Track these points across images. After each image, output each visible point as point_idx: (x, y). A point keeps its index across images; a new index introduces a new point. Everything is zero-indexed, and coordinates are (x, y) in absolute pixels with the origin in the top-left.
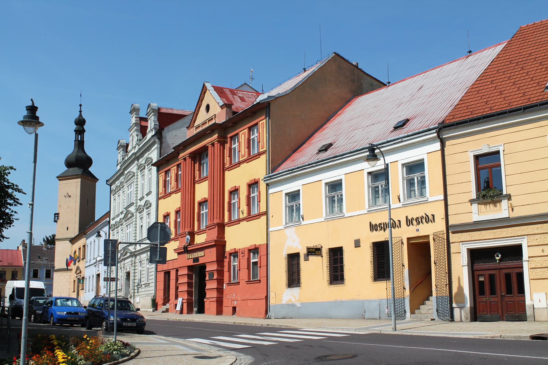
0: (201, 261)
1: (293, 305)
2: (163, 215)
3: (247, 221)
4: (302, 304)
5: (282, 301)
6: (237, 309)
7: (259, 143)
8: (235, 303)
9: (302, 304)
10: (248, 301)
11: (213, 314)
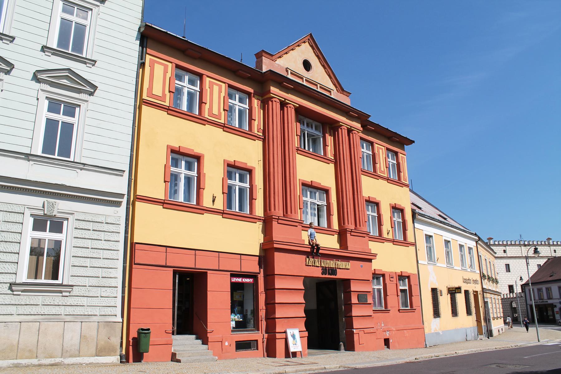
0: (341, 275)
1: (438, 334)
2: (203, 155)
3: (147, 88)
4: (443, 332)
5: (432, 330)
6: (391, 341)
7: (547, 342)
8: (387, 334)
9: (443, 332)
10: (405, 330)
11: (383, 349)
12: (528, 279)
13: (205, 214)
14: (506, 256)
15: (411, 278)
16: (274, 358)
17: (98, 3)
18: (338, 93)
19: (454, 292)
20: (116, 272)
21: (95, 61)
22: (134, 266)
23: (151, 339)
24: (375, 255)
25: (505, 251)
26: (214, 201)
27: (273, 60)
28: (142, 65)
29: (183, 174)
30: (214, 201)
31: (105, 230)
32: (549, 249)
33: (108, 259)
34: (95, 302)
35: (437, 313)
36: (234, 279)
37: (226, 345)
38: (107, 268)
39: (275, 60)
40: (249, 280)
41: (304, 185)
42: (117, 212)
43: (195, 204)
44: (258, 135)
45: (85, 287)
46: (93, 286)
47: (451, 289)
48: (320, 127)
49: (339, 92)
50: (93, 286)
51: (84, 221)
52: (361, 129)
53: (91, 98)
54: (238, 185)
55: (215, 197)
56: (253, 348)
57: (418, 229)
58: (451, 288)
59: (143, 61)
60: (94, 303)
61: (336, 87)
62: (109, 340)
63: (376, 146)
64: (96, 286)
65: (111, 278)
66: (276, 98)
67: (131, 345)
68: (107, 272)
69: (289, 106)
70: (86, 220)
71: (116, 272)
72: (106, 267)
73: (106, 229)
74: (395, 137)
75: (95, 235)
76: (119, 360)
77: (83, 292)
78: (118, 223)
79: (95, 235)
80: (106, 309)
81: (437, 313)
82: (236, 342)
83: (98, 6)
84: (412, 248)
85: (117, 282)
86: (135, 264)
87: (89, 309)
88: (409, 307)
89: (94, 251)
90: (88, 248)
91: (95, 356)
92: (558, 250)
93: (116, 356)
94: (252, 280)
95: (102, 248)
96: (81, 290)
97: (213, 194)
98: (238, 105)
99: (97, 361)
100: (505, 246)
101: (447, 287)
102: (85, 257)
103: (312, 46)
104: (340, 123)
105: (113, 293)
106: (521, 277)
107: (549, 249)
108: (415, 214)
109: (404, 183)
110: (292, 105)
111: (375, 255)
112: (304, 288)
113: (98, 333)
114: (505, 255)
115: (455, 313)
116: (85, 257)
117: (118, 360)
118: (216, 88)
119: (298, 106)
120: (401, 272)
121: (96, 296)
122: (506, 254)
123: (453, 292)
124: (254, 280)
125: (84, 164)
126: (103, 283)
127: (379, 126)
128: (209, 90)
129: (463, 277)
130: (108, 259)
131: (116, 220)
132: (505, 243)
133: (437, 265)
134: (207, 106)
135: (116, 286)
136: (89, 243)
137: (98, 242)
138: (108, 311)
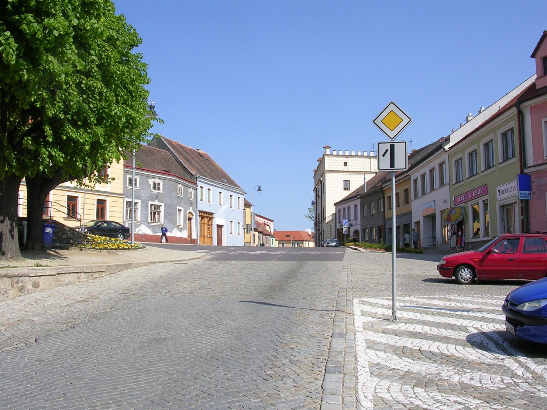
12: (364, 183)
14: (346, 170)
16: (339, 262)
25: (346, 164)
32: (369, 162)
66: (169, 150)
92: (341, 166)
100: (347, 157)
106: (259, 187)
107: (369, 162)
108: (76, 214)
114: (345, 169)
122: (347, 167)
132: (347, 153)
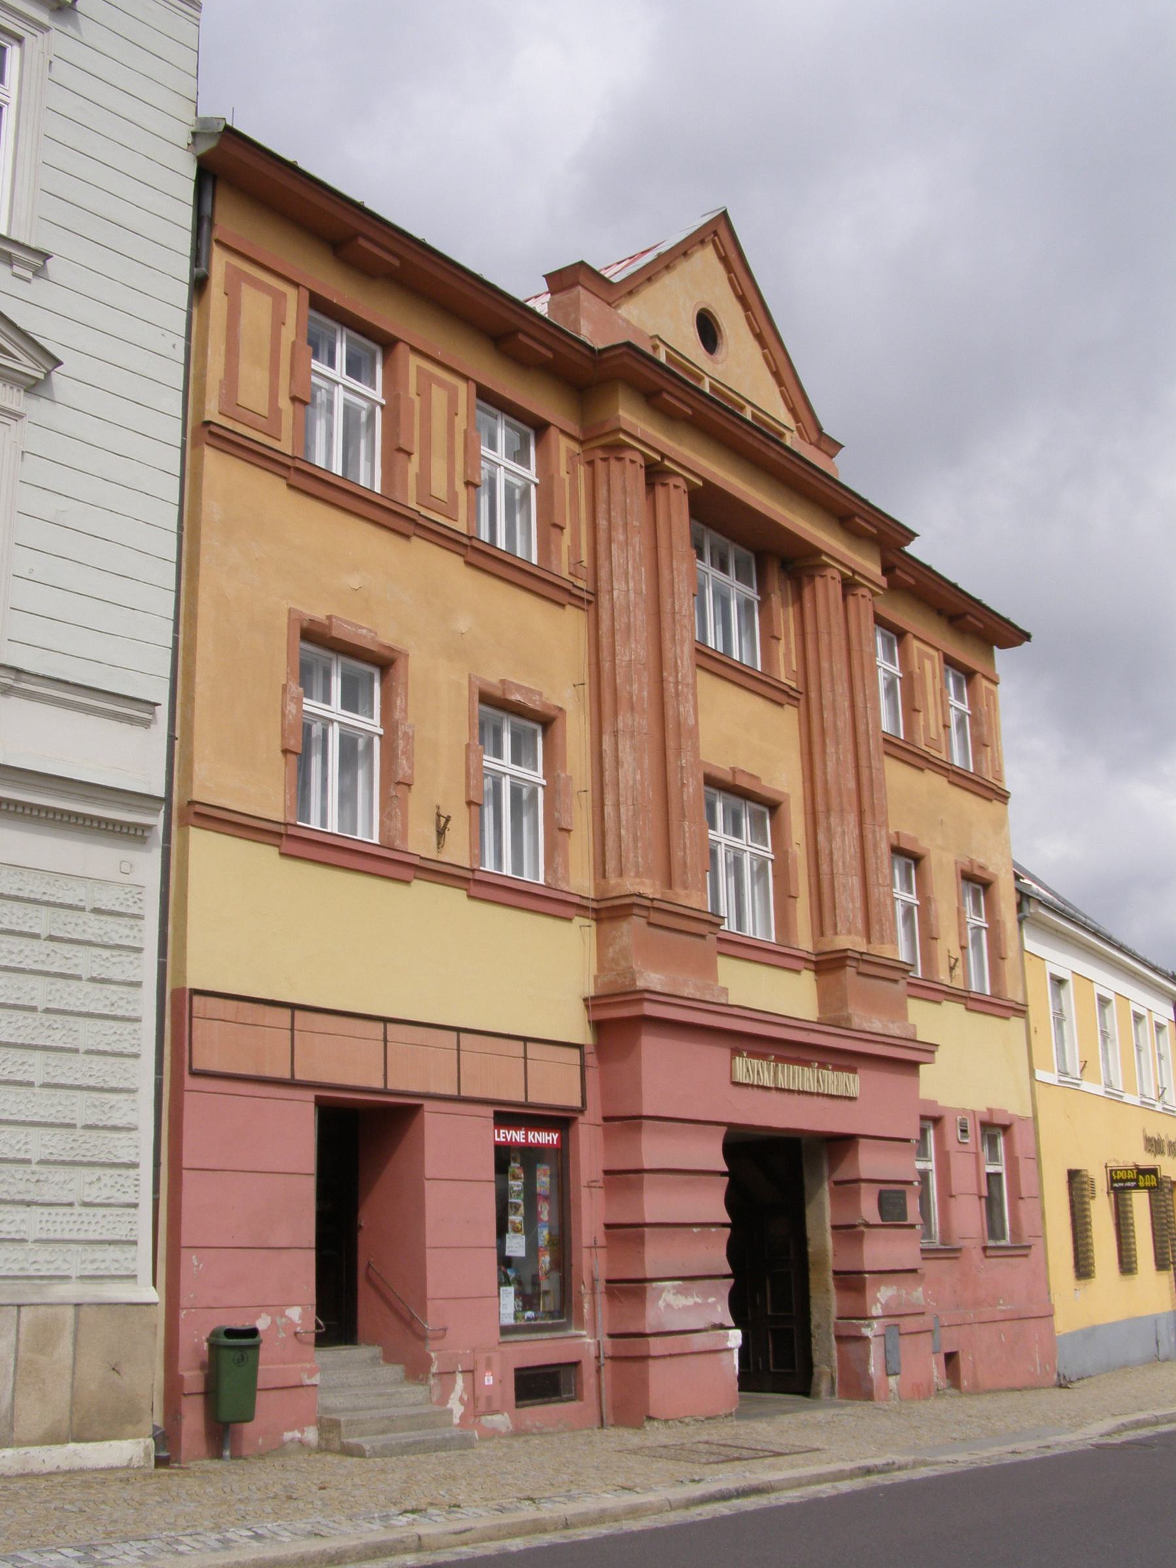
13: (415, 882)
15: (1016, 1129)
17: (43, 17)
18: (802, 441)
19: (1133, 1184)
20: (133, 1106)
21: (46, 254)
22: (189, 1082)
23: (260, 1367)
24: (930, 1049)
26: (441, 833)
27: (611, 301)
28: (199, 285)
29: (336, 724)
30: (441, 833)
31: (93, 939)
33: (104, 1053)
34: (61, 1224)
35: (1083, 1268)
36: (502, 1131)
37: (486, 1383)
38: (102, 1090)
39: (616, 303)
40: (547, 1138)
41: (712, 781)
42: (131, 866)
43: (378, 843)
44: (575, 586)
45: (22, 1167)
46: (55, 1163)
47: (1120, 1175)
48: (749, 564)
49: (804, 440)
50: (55, 1163)
51: (17, 899)
52: (883, 582)
53: (34, 408)
54: (511, 776)
55: (448, 819)
56: (564, 1394)
57: (1032, 957)
58: (1121, 1170)
59: (203, 269)
60: (58, 1227)
61: (797, 419)
62: (116, 1375)
63: (915, 645)
64: (64, 1163)
65: (115, 1128)
67: (584, 1250)
68: (103, 1104)
69: (672, 481)
70: (25, 894)
71: (133, 1106)
72: (99, 1085)
73: (93, 934)
74: (972, 615)
75: (59, 959)
76: (150, 1455)
77: (22, 1186)
78: (134, 910)
79: (59, 959)
80: (99, 1253)
81: (1083, 1268)
82: (517, 1370)
83: (45, 28)
84: (1016, 1023)
85: (137, 1147)
86: (195, 1074)
87: (44, 1254)
88: (1008, 1238)
89: (55, 1021)
90: (33, 1009)
91: (68, 1442)
93: (141, 1440)
94: (556, 1136)
95: (83, 1009)
96: (13, 1177)
97: (438, 808)
98: (505, 468)
99: (77, 1463)
101: (1106, 1167)
102: (23, 1046)
103: (724, 260)
104: (824, 558)
105: (123, 1190)
109: (995, 788)
110: (836, 570)
111: (930, 1049)
112: (726, 1169)
113: (75, 1349)
115: (1127, 1265)
116: (23, 1046)
117: (147, 1455)
118: (439, 397)
119: (700, 483)
120: (990, 1111)
121: (65, 1200)
123: (1128, 1184)
124: (560, 1139)
125: (18, 671)
126: (88, 1150)
127: (929, 574)
128: (567, 477)
129: (1144, 1130)
130: (104, 1053)
131: (128, 900)
133: (1082, 1088)
134: (414, 466)
135: (134, 1159)
136: (38, 992)
137: (69, 986)
138: (109, 1260)
